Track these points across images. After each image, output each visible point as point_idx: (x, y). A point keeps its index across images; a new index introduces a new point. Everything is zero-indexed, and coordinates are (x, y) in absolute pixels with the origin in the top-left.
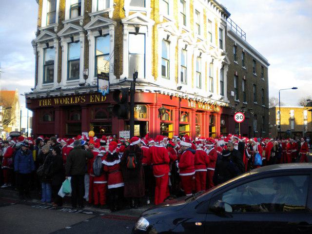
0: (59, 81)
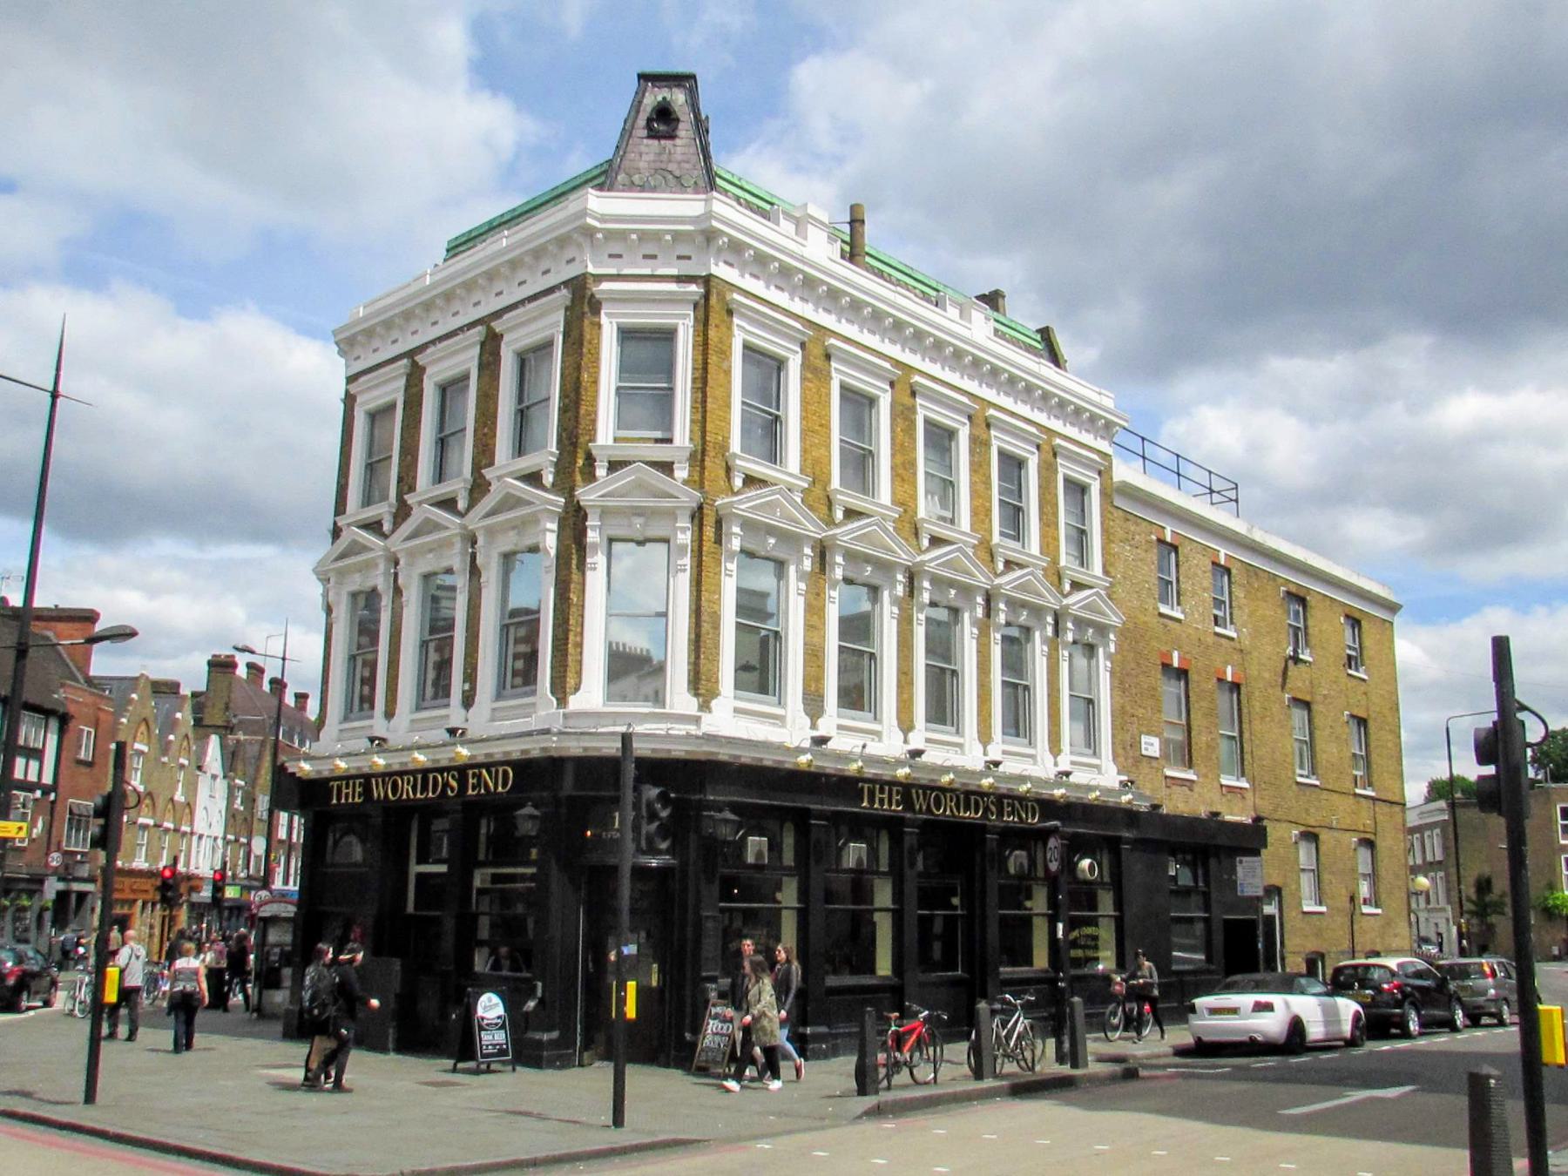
0: (389, 714)
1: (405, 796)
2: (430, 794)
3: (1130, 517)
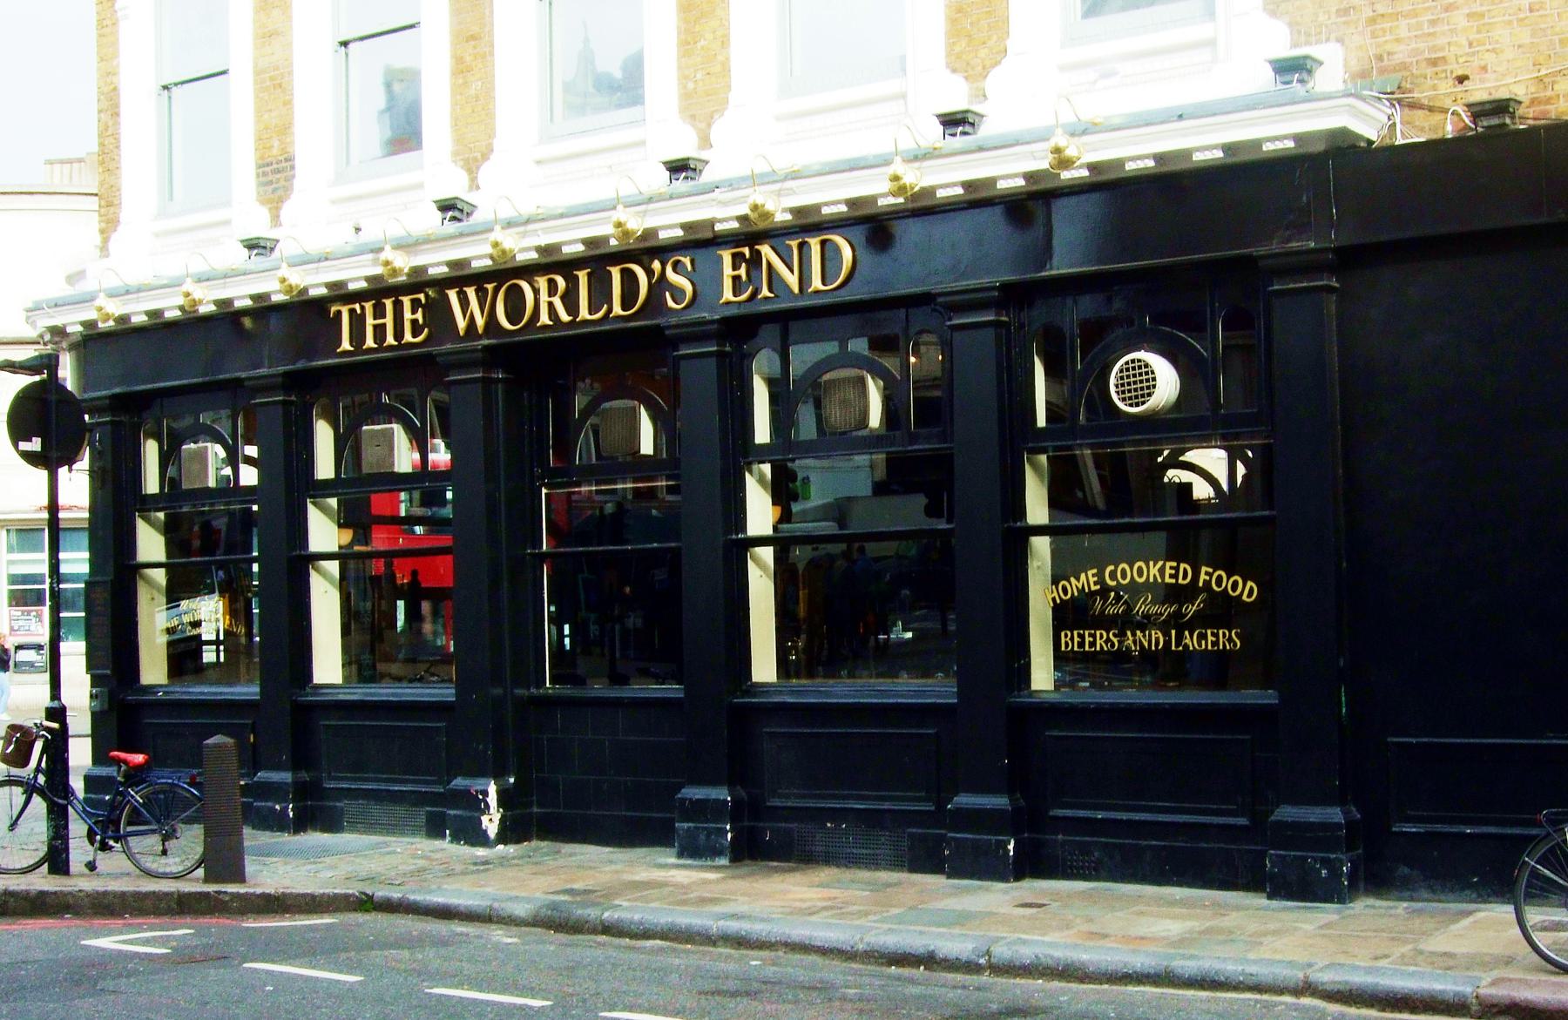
1: (544, 319)
2: (617, 310)
3: (892, 323)
